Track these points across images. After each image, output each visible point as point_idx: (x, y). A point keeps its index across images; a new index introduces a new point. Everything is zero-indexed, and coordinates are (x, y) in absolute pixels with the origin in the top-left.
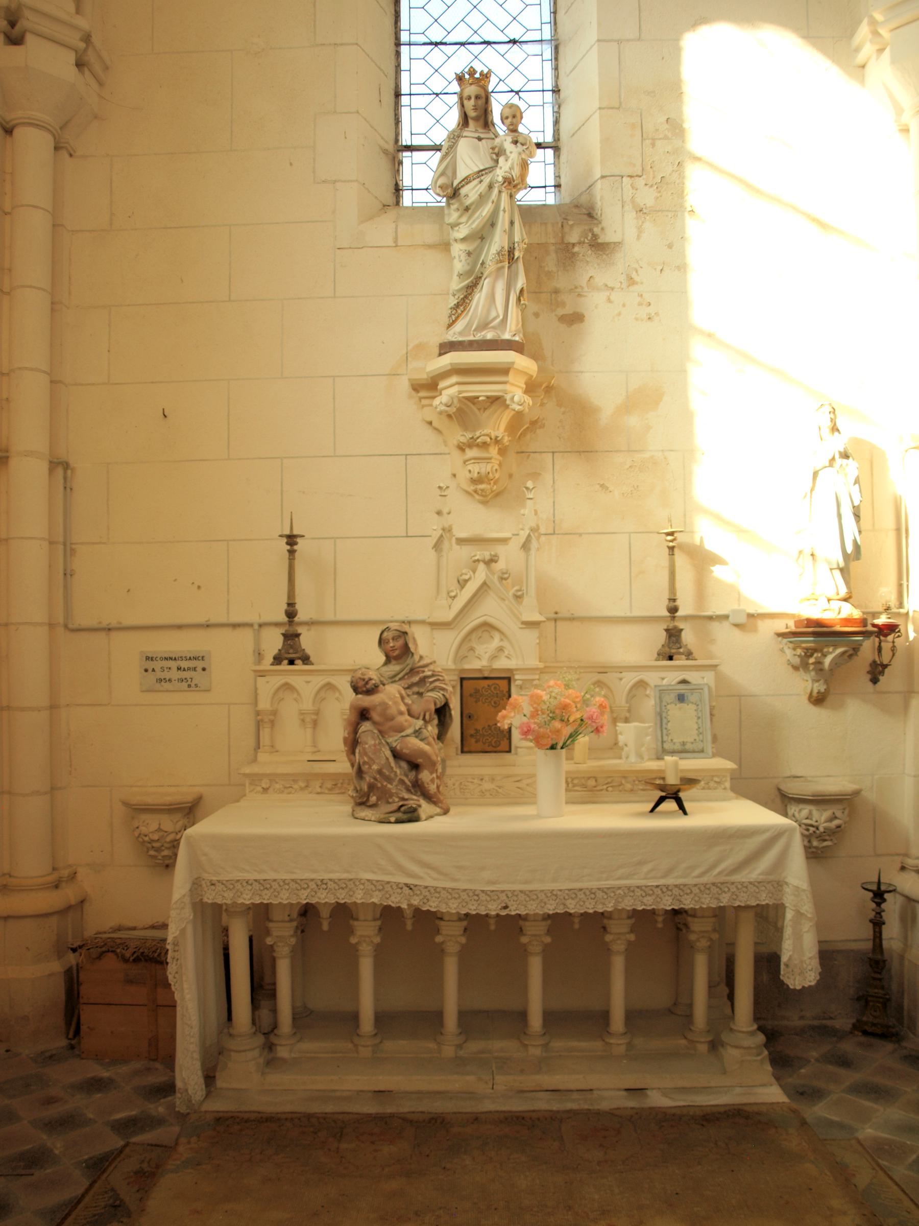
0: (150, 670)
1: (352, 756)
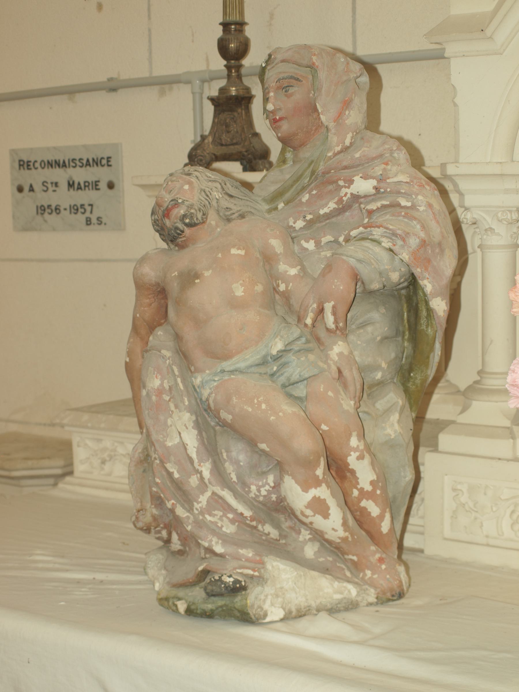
0: (26, 188)
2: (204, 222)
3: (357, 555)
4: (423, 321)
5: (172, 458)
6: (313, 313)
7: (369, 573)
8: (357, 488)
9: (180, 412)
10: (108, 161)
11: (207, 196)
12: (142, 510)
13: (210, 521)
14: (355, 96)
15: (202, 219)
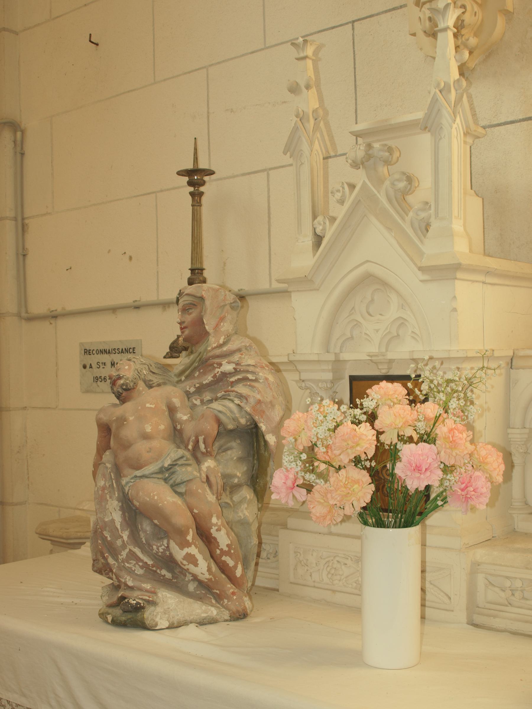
0: (88, 366)
2: (134, 388)
3: (219, 590)
4: (262, 448)
5: (107, 528)
6: (193, 443)
7: (226, 601)
8: (219, 549)
9: (112, 500)
10: (133, 350)
11: (139, 373)
12: (96, 560)
13: (128, 566)
14: (228, 315)
15: (133, 386)
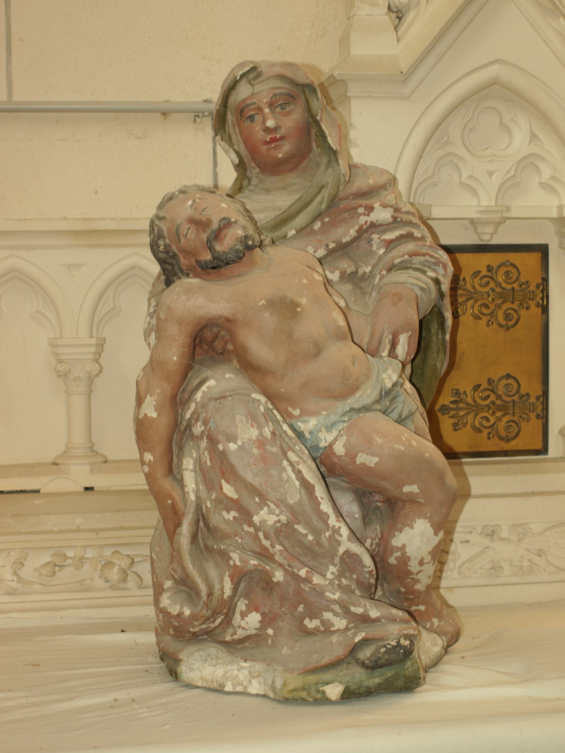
1: (167, 484)
7: (435, 621)
